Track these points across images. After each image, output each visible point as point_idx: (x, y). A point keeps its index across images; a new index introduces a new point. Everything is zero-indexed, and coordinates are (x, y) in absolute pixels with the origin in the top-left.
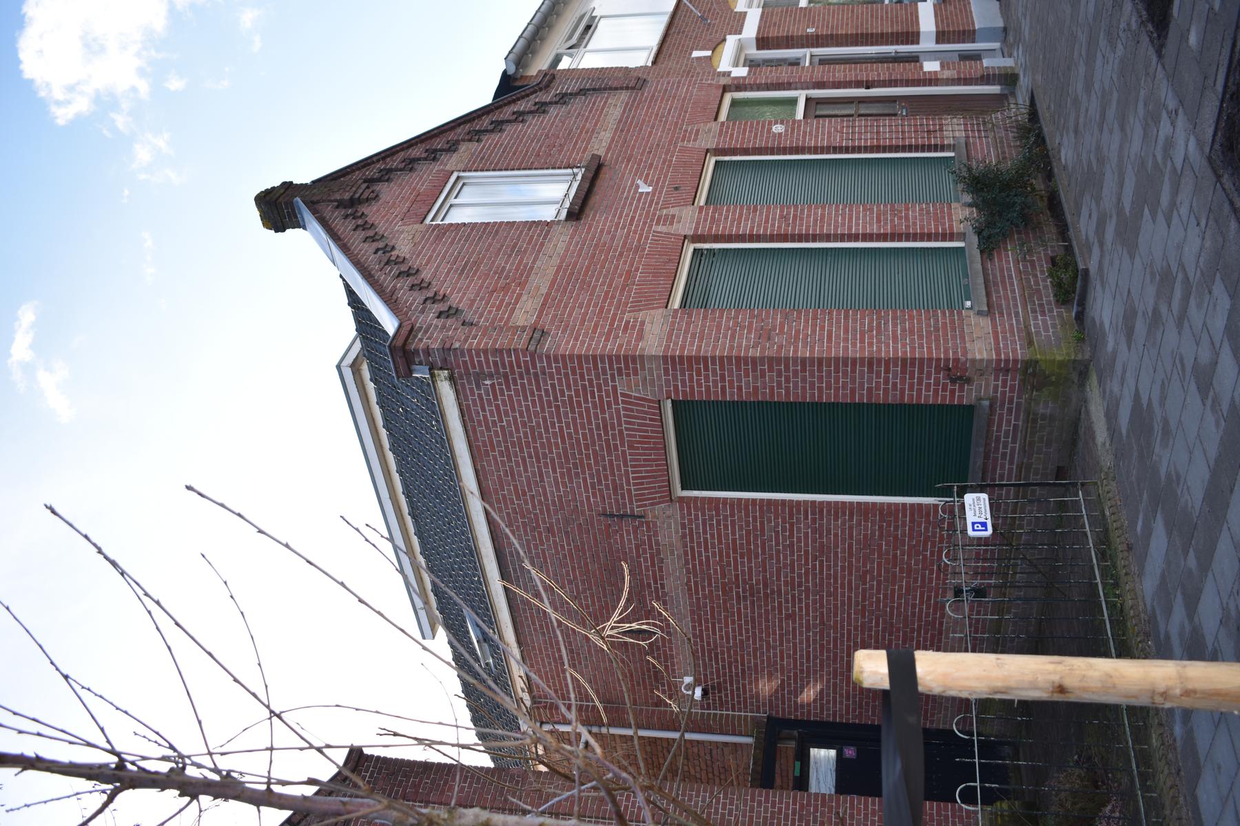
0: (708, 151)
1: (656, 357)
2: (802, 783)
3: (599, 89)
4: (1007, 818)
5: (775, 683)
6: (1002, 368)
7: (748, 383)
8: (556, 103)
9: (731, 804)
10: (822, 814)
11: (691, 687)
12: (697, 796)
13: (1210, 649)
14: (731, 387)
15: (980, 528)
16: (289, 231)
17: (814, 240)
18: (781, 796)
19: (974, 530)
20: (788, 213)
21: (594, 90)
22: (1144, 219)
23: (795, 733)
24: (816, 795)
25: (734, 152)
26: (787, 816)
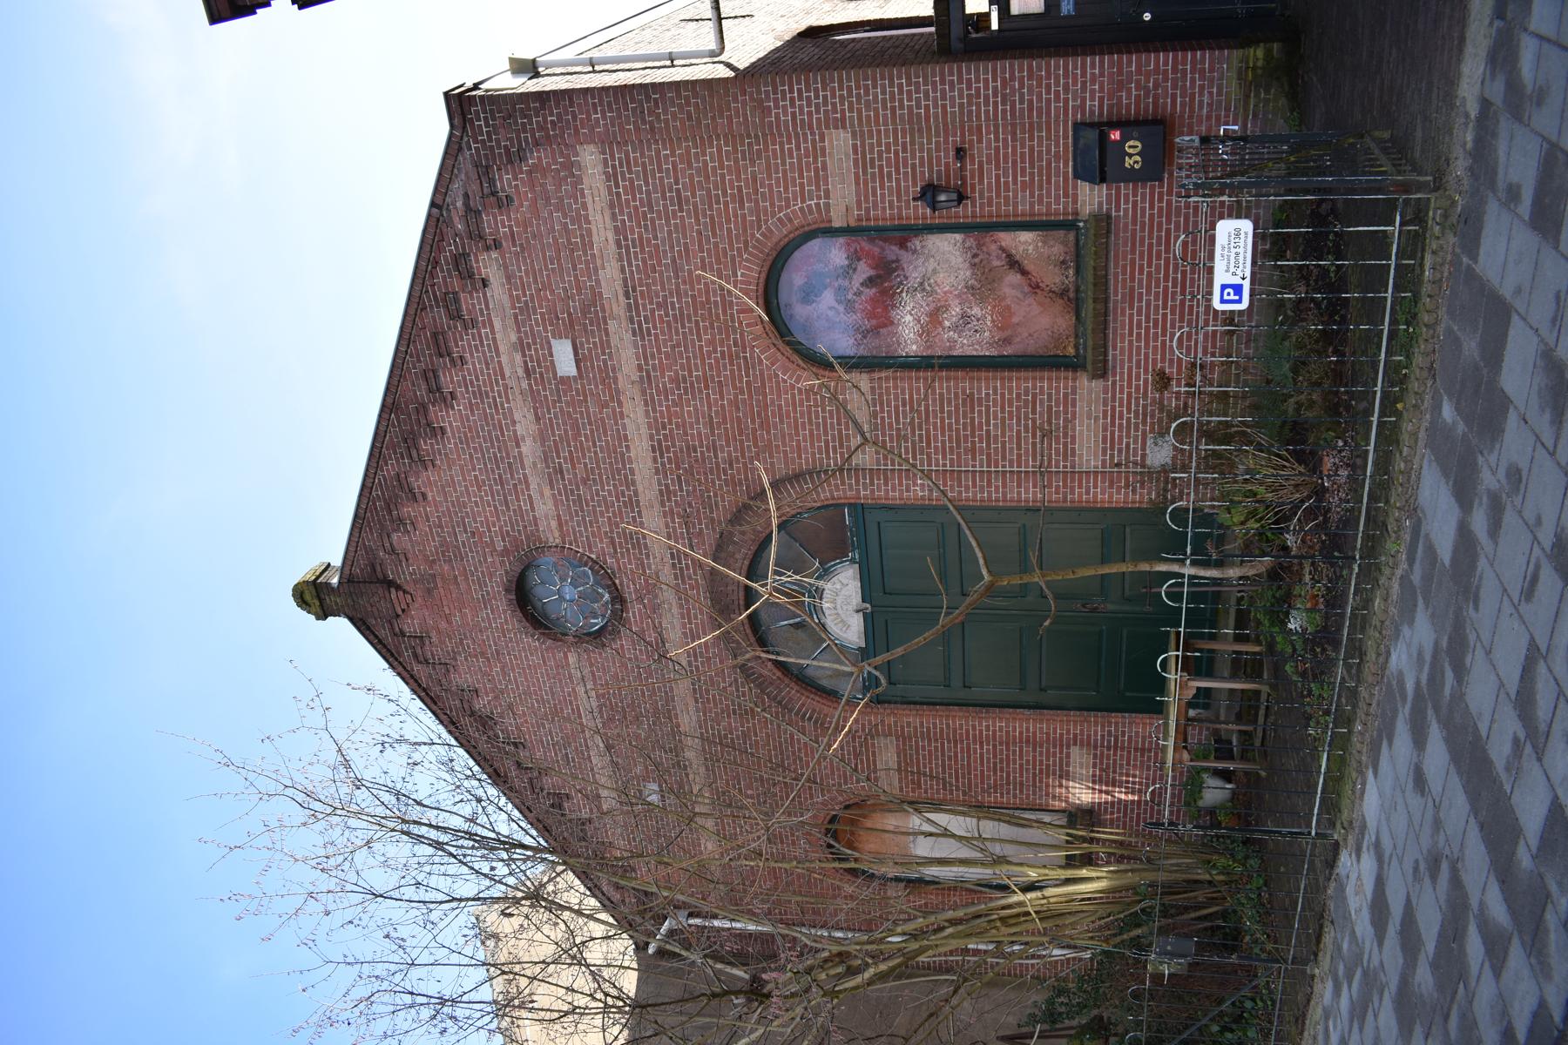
4: (1259, 72)
9: (918, 92)
12: (875, 87)
15: (1232, 297)
18: (977, 71)
19: (1223, 301)
22: (1435, 930)
26: (987, 97)
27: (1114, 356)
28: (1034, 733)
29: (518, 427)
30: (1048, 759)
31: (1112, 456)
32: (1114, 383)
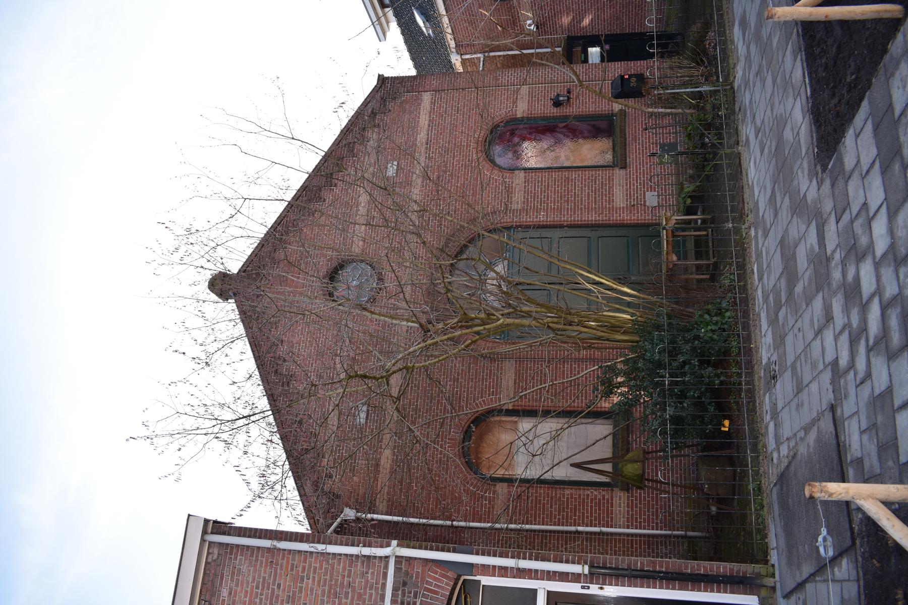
2: (586, 61)
5: (570, 18)
10: (595, 72)
11: (530, 25)
13: (764, 362)
23: (581, 42)
24: (592, 64)
27: (630, 161)
32: (630, 171)
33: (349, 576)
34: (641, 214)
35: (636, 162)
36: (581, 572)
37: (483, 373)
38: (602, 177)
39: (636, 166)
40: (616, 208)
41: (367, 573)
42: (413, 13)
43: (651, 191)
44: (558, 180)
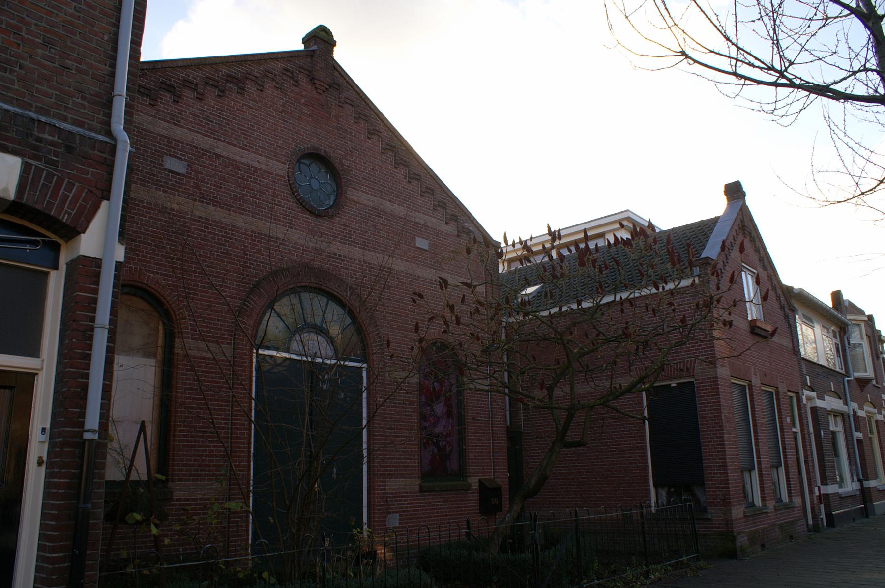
0: (777, 388)
1: (716, 374)
3: (792, 334)
6: (728, 522)
7: (708, 414)
8: (785, 314)
14: (705, 407)
16: (725, 197)
17: (755, 439)
20: (763, 427)
21: (791, 331)
25: (778, 400)
27: (426, 495)
28: (239, 456)
29: (397, 206)
30: (214, 466)
31: (390, 497)
32: (417, 496)
33: (78, 70)
34: (380, 510)
35: (426, 502)
36: (86, 428)
37: (218, 320)
38: (413, 466)
39: (422, 503)
40: (385, 482)
41: (83, 98)
42: (535, 285)
43: (400, 519)
44: (410, 419)
